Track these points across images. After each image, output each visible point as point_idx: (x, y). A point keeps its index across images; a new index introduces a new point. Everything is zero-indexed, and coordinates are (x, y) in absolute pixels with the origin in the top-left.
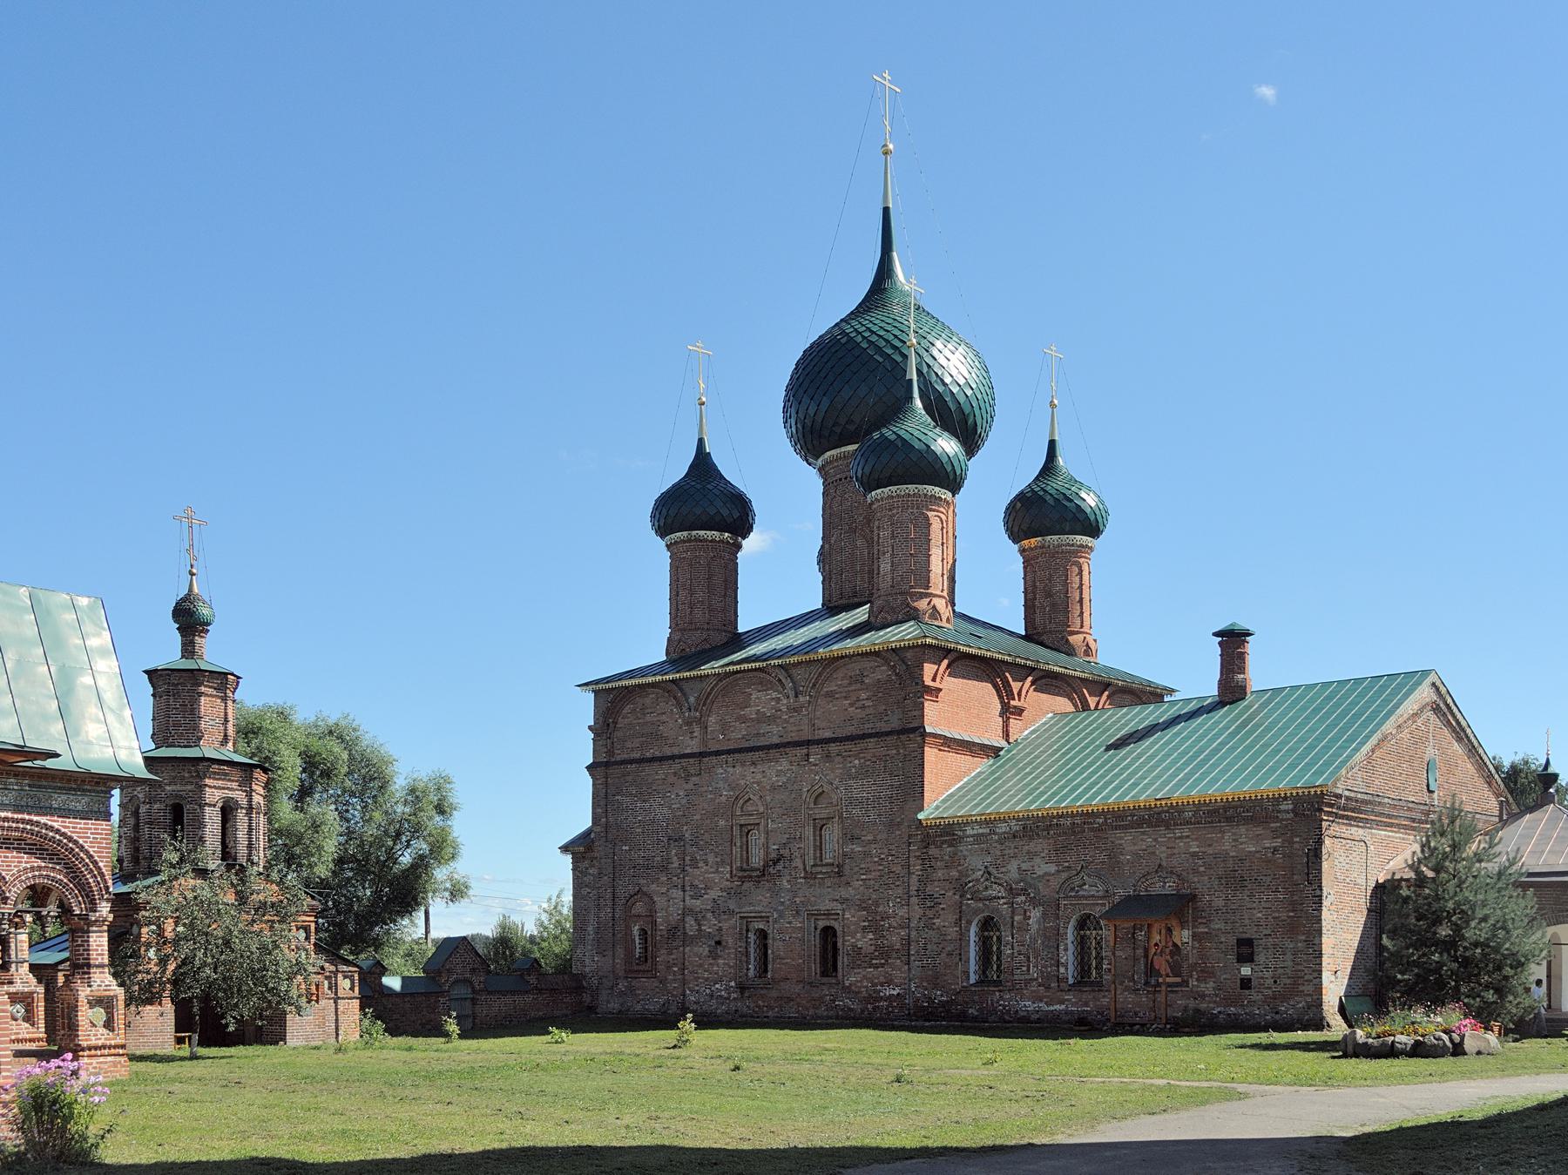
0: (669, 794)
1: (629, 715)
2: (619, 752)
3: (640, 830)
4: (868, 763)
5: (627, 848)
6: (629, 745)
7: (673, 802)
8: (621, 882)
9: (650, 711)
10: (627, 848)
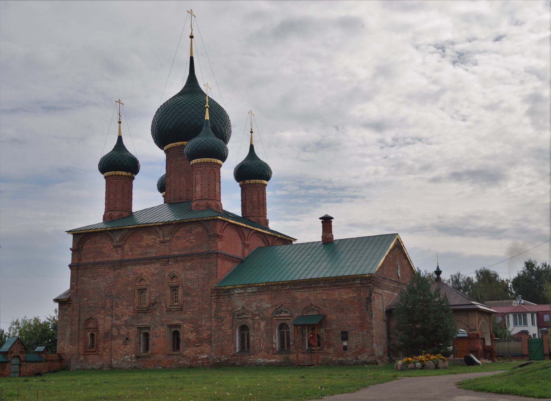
0: (106, 277)
1: (89, 244)
5: (86, 299)
7: (108, 280)
10: (86, 299)
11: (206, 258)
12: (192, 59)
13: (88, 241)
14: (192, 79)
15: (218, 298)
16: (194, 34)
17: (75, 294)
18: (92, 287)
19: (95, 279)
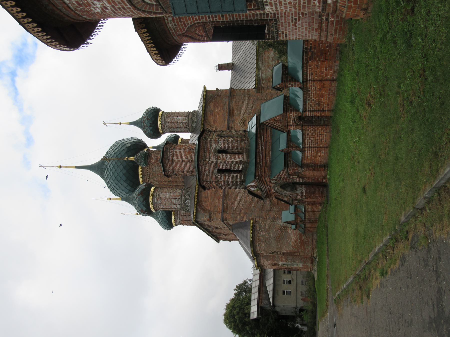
1: (207, 204)
2: (219, 209)
3: (247, 198)
4: (237, 107)
5: (253, 204)
6: (217, 204)
8: (265, 208)
9: (207, 194)
10: (253, 204)
11: (234, 98)
12: (77, 167)
13: (204, 204)
14: (91, 168)
15: (264, 88)
16: (58, 165)
17: (247, 216)
18: (243, 198)
19: (237, 194)
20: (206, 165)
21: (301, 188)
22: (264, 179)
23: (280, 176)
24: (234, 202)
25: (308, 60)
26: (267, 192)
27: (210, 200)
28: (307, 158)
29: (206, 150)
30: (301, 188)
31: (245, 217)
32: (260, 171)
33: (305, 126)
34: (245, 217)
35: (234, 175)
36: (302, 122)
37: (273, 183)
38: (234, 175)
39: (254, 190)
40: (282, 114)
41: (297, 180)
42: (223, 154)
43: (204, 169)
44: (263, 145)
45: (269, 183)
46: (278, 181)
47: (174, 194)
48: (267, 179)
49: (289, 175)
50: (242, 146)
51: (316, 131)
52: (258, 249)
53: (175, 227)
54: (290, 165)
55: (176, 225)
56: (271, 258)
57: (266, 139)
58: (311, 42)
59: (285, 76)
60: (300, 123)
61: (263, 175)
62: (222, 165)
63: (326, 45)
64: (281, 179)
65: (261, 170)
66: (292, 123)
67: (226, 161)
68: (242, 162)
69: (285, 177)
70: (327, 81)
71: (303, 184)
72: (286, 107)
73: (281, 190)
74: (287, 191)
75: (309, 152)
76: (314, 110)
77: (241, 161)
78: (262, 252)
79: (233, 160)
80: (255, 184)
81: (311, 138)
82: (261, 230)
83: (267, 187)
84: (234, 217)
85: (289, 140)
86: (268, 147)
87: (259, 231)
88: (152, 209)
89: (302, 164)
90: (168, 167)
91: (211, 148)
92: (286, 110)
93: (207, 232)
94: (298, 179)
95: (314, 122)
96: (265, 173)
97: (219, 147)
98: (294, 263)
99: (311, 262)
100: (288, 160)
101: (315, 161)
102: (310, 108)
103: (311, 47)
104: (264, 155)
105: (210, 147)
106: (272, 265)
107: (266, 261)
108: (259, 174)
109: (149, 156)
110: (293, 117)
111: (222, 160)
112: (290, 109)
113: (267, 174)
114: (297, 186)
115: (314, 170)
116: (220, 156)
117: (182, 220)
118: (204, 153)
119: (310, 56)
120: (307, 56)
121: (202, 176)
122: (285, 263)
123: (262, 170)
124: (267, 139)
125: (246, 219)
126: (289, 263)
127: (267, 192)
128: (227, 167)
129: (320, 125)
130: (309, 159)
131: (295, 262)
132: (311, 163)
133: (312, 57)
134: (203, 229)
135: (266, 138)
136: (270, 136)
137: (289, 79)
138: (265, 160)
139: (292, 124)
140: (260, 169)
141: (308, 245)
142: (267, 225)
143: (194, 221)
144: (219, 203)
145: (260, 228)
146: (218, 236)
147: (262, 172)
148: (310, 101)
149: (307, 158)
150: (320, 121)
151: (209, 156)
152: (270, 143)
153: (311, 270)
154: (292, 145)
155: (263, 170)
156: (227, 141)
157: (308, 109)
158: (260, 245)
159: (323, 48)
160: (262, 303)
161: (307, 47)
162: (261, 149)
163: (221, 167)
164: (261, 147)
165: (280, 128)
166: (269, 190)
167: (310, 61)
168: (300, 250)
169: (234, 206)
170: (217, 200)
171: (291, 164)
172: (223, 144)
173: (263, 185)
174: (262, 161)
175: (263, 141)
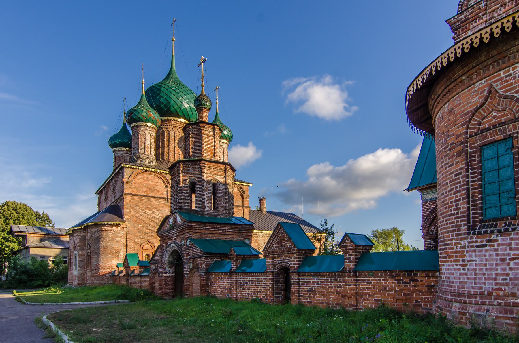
2: (136, 191)
3: (148, 220)
20: (200, 170)
21: (171, 271)
22: (186, 231)
23: (192, 249)
24: (144, 207)
25: (397, 278)
26: (167, 236)
27: (145, 184)
28: (219, 278)
29: (216, 171)
30: (171, 271)
31: (128, 217)
32: (197, 227)
33: (273, 275)
34: (128, 217)
35: (188, 199)
36: (277, 272)
37: (181, 242)
38: (188, 199)
39: (170, 222)
40: (401, 235)
41: (186, 267)
42: (212, 189)
43: (195, 167)
44: (224, 231)
45: (181, 238)
46: (185, 247)
47: (150, 148)
48: (187, 235)
49: (194, 259)
50: (220, 209)
51: (263, 288)
52: (93, 230)
53: (111, 151)
54: (208, 260)
55: (114, 151)
56: (83, 244)
57: (229, 234)
58: (424, 281)
59: (361, 250)
60: (276, 269)
61: (192, 231)
62: (200, 187)
63: (420, 300)
64: (187, 250)
65: (198, 228)
66: (278, 260)
67: (204, 191)
68: (204, 209)
69: (190, 254)
70: (355, 301)
71: (175, 274)
72: (303, 252)
73: (171, 251)
74: (169, 257)
75: (228, 280)
76: (301, 285)
77: (205, 207)
78: (89, 234)
79: (206, 199)
80: (179, 222)
81: (251, 282)
82: (114, 232)
83: (175, 235)
84: (127, 206)
85: (244, 257)
86: (222, 236)
87: (113, 231)
88: (133, 124)
89: (209, 272)
90: (195, 129)
91: (218, 176)
92: (301, 252)
93: (109, 180)
94: (188, 269)
95: (278, 286)
96: (195, 232)
97: (219, 185)
98: (77, 267)
99: (79, 283)
100: (214, 257)
101: (215, 286)
102: (304, 281)
103: (417, 281)
104: (213, 232)
105: (219, 175)
106: (74, 245)
107: (80, 239)
108: (193, 225)
109: (206, 110)
110: (287, 261)
111: (206, 187)
112: (301, 257)
113: (193, 235)
114: (173, 268)
115: (202, 286)
116: (210, 185)
117: (119, 157)
118: (213, 168)
119: (402, 280)
120: (404, 276)
121: (187, 165)
122: (77, 257)
123: (198, 229)
124: (229, 235)
125: (126, 218)
126: (77, 262)
127: (167, 236)
128: (199, 192)
129: (273, 293)
130: (217, 280)
131: (79, 267)
132: (211, 282)
133: (401, 282)
134: (113, 175)
135: (231, 235)
136: (233, 239)
137: (358, 254)
138: (208, 233)
139: (276, 260)
140: (198, 228)
141: (99, 280)
142: (120, 239)
143: (122, 165)
144: (142, 192)
145: (116, 232)
146: (104, 192)
147: (196, 229)
148: (317, 281)
149: (219, 278)
150: (279, 293)
151: (209, 174)
152: (226, 238)
153: (69, 283)
154: (239, 260)
155: (198, 231)
156: (225, 194)
157: (302, 278)
158: (98, 232)
159: (414, 296)
160: (29, 237)
161: (418, 275)
162: (219, 229)
163: (197, 186)
164: (221, 229)
165: (270, 246)
166: (171, 238)
167: (395, 280)
168: (93, 272)
169: (139, 207)
170: (145, 190)
171: (209, 260)
172: (222, 190)
173: (178, 231)
174: (207, 230)
175: (227, 231)
